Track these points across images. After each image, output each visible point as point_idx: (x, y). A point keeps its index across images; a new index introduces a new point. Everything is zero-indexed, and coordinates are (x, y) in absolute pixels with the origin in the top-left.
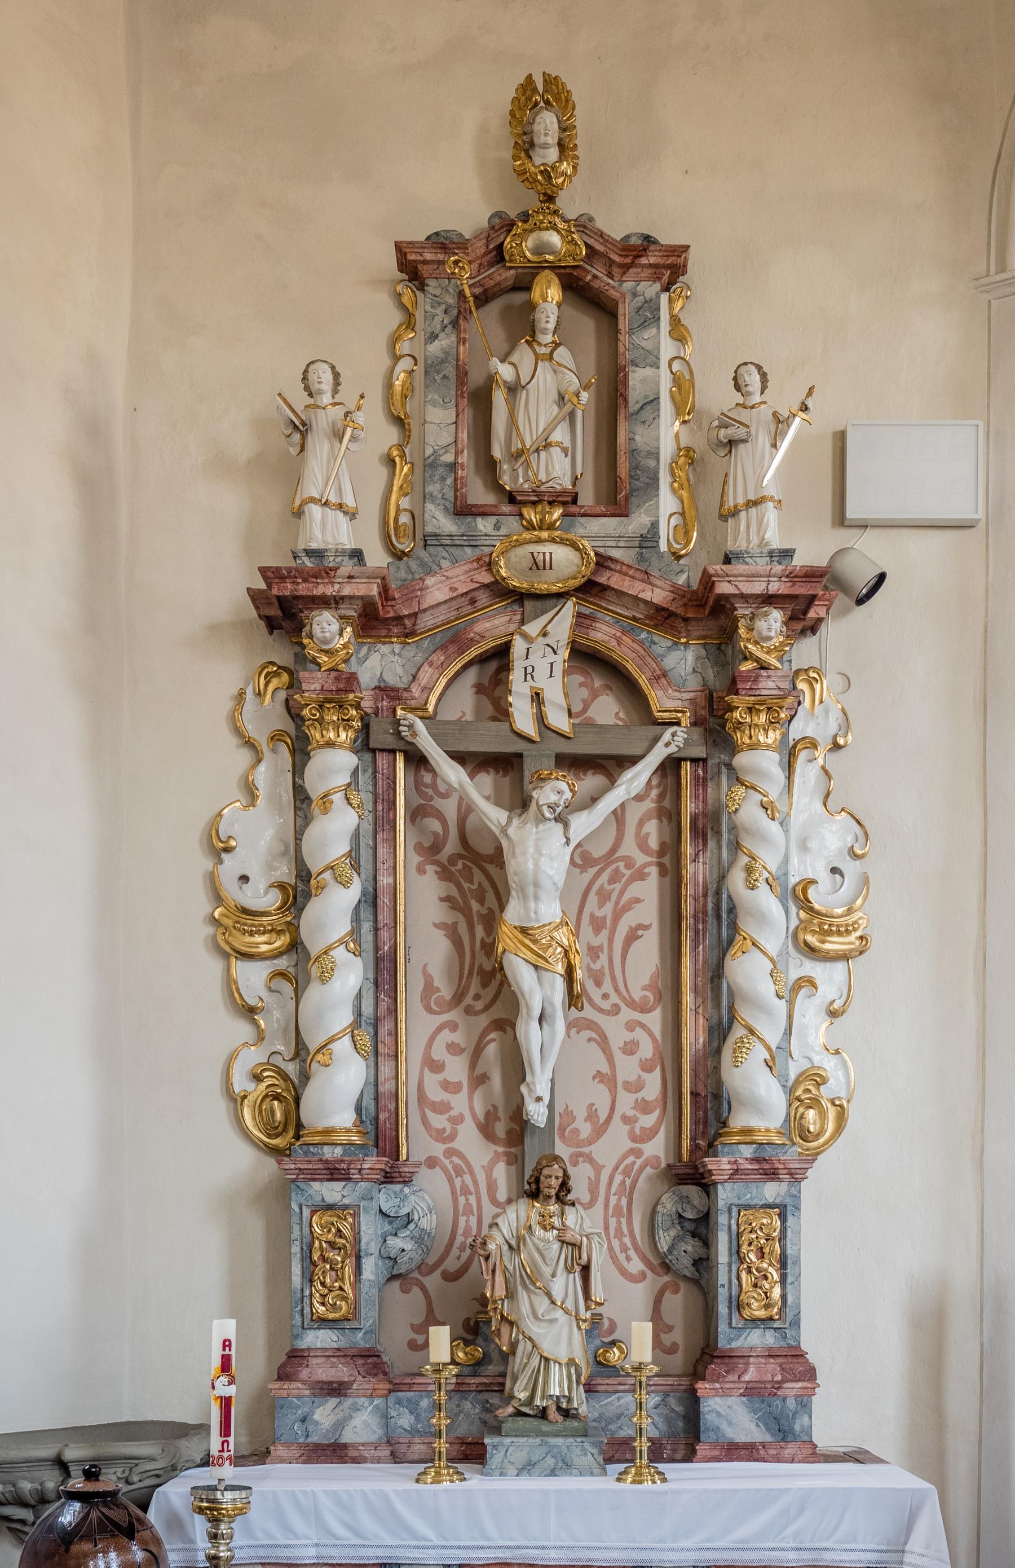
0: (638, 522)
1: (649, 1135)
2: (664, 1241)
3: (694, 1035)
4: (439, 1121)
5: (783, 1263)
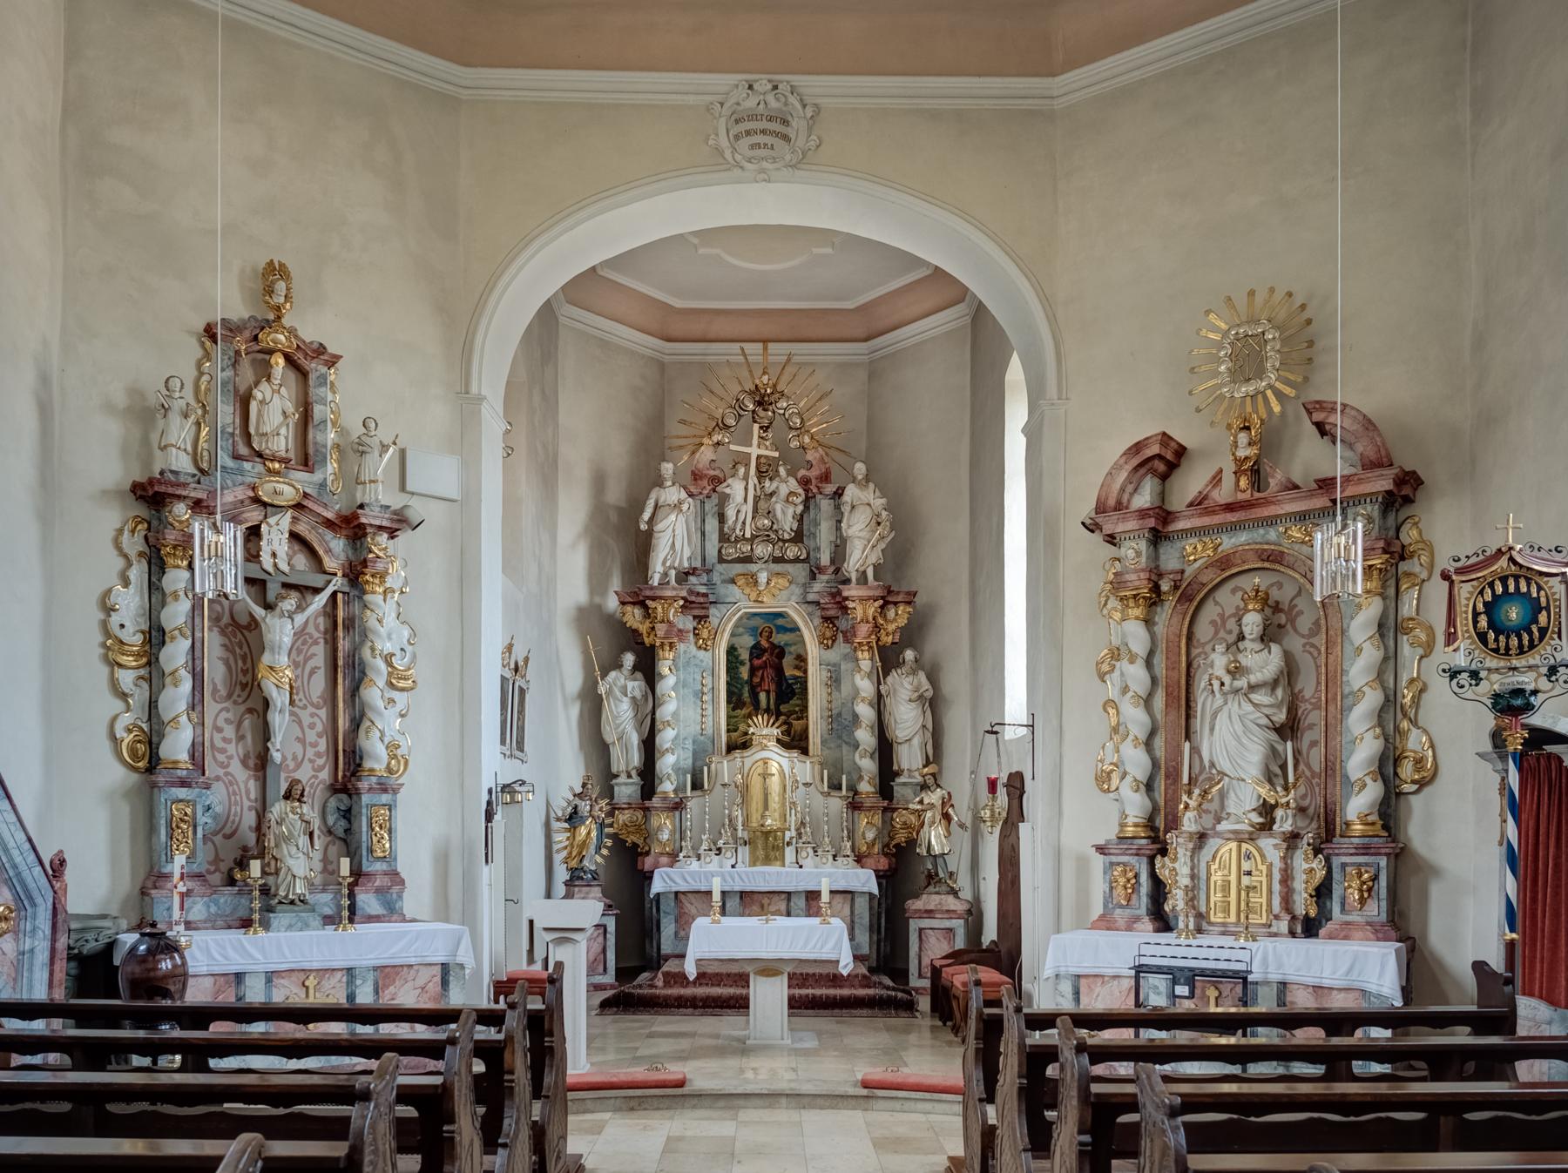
0: (317, 477)
1: (321, 768)
2: (331, 820)
3: (343, 723)
4: (221, 758)
5: (390, 832)
